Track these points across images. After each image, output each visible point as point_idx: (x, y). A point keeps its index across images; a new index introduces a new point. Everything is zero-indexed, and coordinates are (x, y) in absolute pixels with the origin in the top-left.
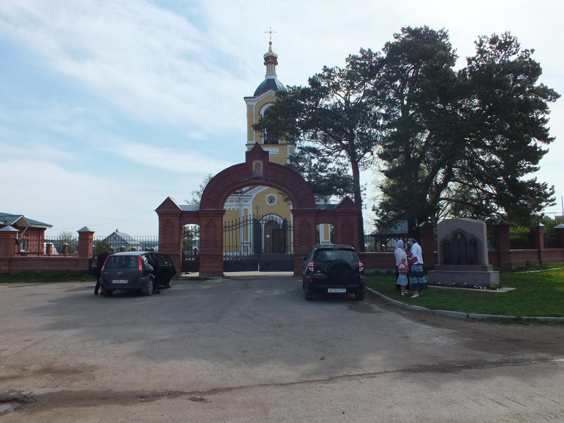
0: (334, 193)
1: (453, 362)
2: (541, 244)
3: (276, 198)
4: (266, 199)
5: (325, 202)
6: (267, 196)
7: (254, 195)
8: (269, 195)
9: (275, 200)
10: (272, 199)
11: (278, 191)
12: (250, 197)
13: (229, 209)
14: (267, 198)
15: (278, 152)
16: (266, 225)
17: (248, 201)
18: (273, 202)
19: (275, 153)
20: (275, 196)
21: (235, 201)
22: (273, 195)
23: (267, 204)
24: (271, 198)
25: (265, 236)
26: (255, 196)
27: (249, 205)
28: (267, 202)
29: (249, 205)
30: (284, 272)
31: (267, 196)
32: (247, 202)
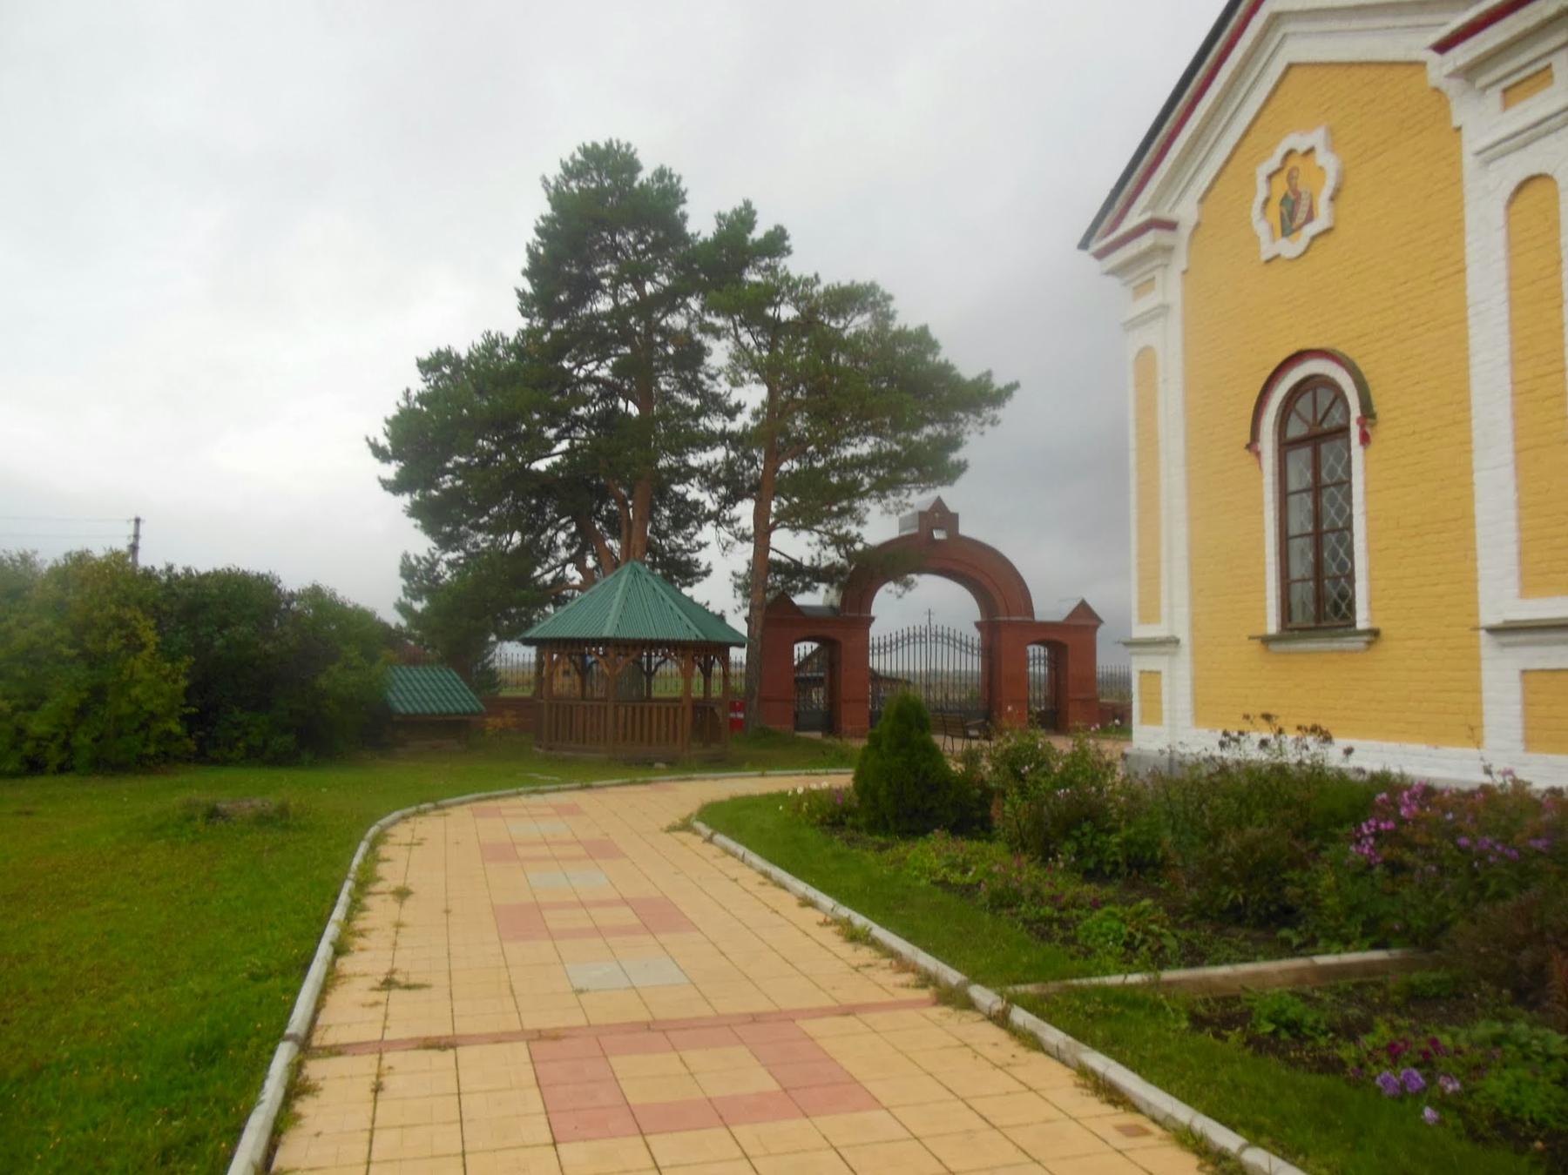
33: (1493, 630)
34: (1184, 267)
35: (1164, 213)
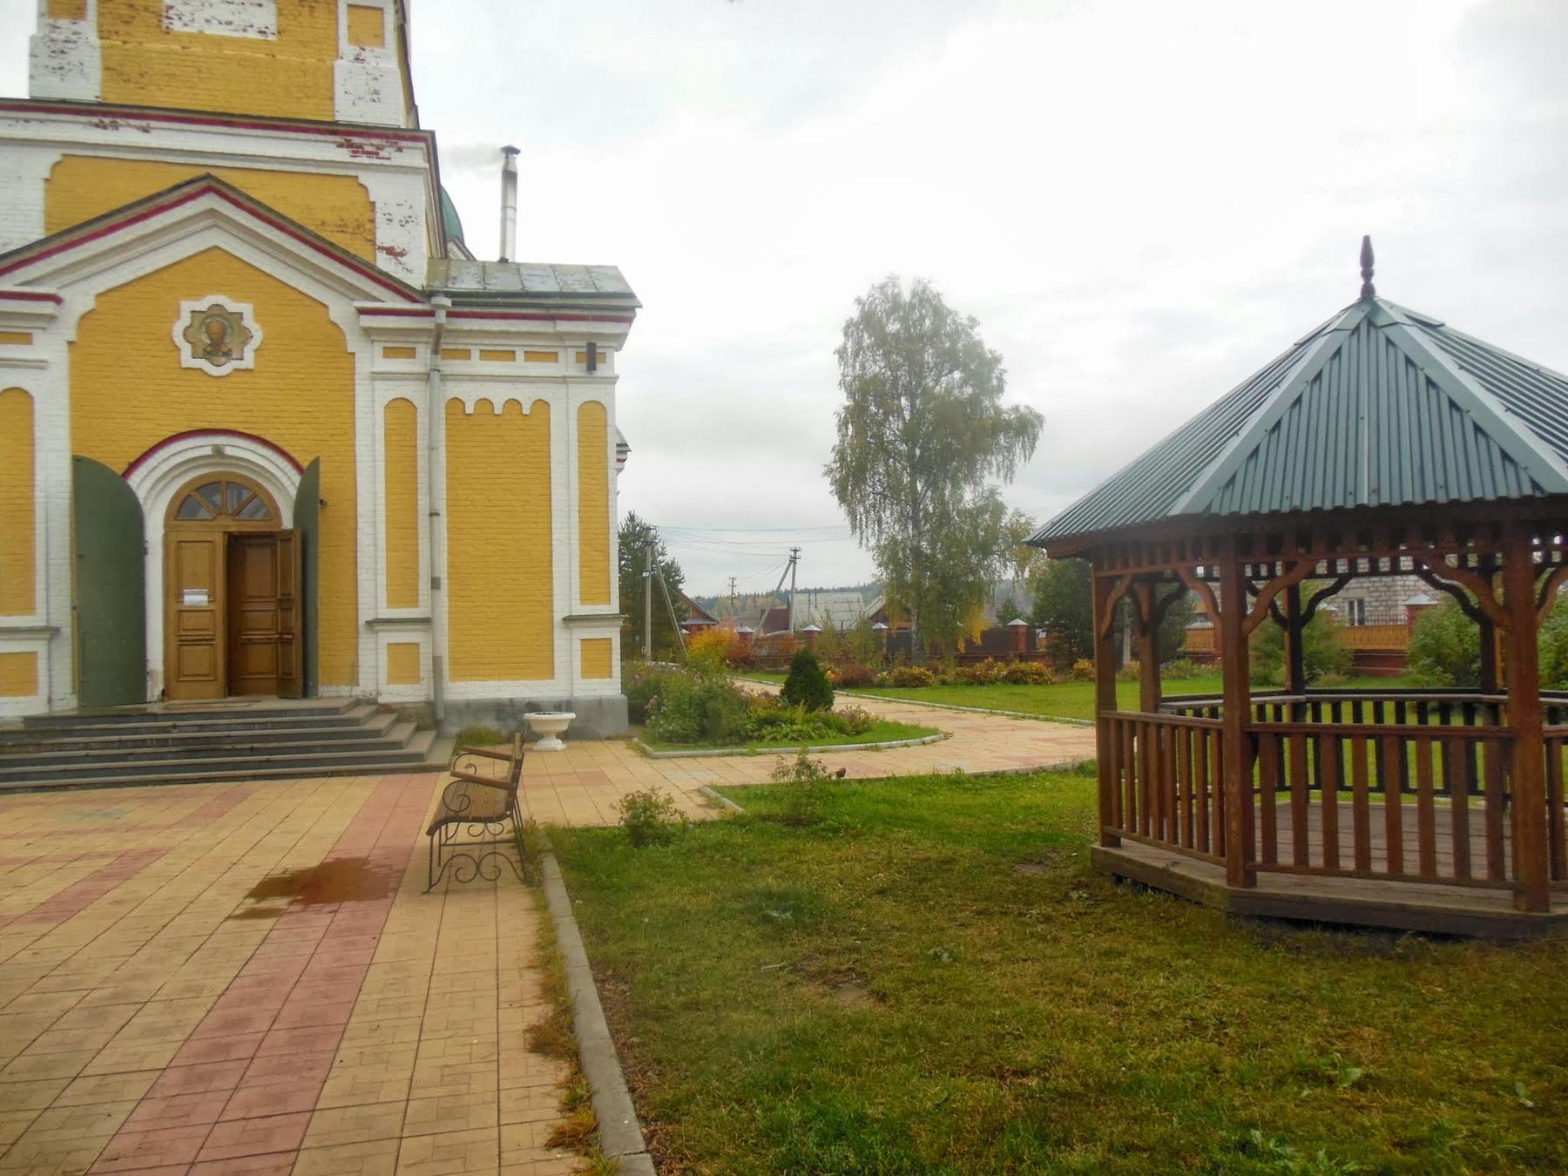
0: (924, 347)
1: (1112, 930)
2: (492, 683)
3: (249, 322)
4: (255, 343)
5: (584, 366)
6: (187, 306)
7: (80, 299)
8: (203, 305)
9: (246, 336)
10: (223, 332)
11: (601, 291)
12: (47, 308)
13: (485, 402)
14: (185, 320)
15: (273, 29)
16: (181, 509)
17: (35, 340)
18: (228, 354)
19: (252, 35)
20: (246, 309)
21: (520, 355)
22: (231, 306)
23: (187, 359)
24: (215, 327)
25: (173, 592)
26: (89, 303)
27: (40, 365)
28: (186, 349)
29: (40, 365)
30: (1534, 447)
31: (187, 306)
32: (26, 339)
33: (370, 624)
34: (73, 337)
35: (62, 294)
